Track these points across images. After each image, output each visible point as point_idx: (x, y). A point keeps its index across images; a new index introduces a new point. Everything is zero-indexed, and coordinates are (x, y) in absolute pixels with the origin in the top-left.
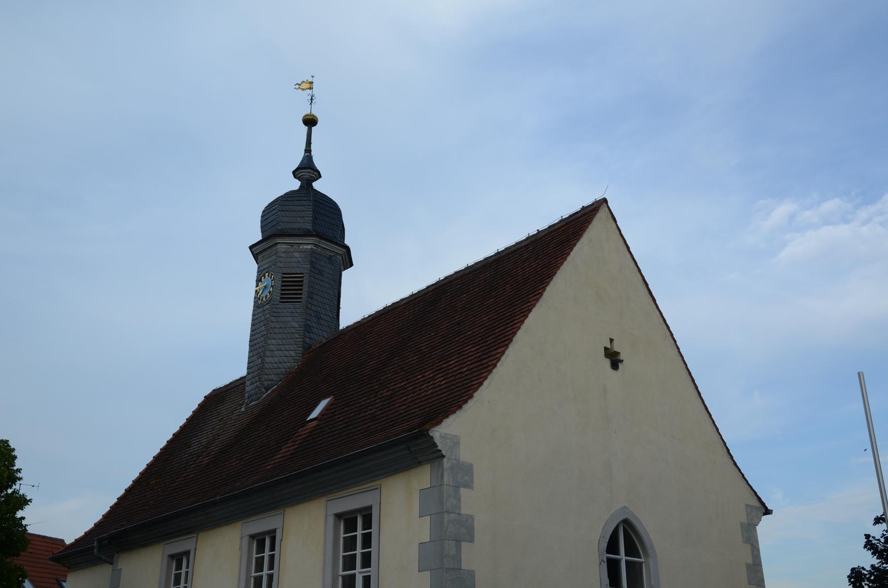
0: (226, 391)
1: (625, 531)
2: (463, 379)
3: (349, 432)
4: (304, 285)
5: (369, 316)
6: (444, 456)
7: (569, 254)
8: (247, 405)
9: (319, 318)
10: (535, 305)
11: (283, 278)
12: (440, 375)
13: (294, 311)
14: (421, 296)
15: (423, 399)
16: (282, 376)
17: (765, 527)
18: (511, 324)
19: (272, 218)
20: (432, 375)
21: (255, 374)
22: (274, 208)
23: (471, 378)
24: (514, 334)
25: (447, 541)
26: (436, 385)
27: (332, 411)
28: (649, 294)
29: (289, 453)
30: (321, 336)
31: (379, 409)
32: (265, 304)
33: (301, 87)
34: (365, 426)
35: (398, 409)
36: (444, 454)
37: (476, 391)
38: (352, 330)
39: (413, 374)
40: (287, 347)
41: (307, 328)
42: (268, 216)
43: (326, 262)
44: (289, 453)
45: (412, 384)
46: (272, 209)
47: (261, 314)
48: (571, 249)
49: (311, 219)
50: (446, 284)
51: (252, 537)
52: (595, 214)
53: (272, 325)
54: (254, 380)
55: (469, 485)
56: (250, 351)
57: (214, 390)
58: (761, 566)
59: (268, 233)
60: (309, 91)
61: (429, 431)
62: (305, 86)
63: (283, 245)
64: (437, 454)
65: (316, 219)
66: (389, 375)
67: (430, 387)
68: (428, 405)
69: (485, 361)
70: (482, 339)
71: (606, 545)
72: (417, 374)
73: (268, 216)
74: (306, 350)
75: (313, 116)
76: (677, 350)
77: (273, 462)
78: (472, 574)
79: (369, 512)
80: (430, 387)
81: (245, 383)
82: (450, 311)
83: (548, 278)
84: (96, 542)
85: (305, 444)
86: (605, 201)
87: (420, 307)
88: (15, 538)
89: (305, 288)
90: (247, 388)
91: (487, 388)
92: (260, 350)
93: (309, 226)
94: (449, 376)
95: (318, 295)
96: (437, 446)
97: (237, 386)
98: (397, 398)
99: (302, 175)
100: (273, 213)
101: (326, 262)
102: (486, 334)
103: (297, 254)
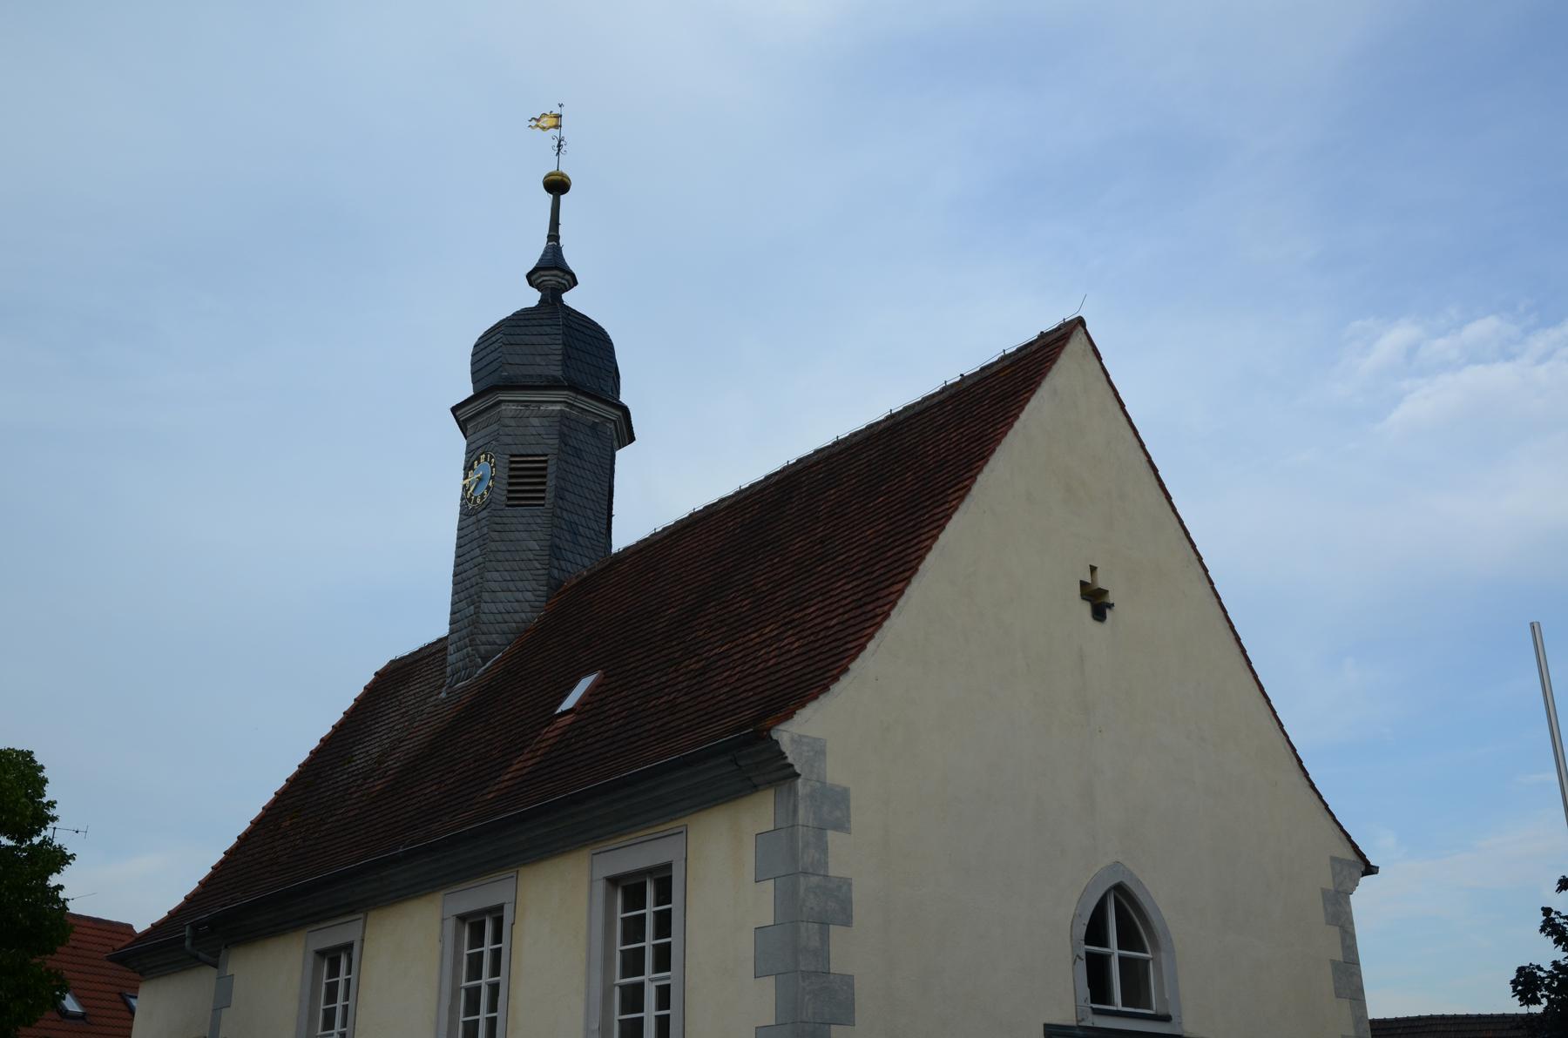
0: (412, 663)
3: (630, 733)
4: (549, 476)
5: (664, 529)
6: (798, 775)
7: (1016, 417)
8: (450, 687)
9: (575, 533)
13: (531, 521)
14: (756, 494)
15: (760, 675)
17: (1365, 897)
19: (491, 357)
20: (775, 633)
22: (494, 339)
25: (805, 924)
30: (579, 564)
31: (683, 692)
32: (480, 509)
33: (540, 124)
36: (798, 771)
40: (520, 584)
41: (555, 551)
42: (484, 352)
44: (525, 771)
45: (740, 648)
48: (1022, 408)
50: (799, 471)
51: (462, 918)
52: (1064, 345)
53: (493, 546)
55: (842, 826)
56: (455, 593)
58: (1359, 964)
59: (483, 385)
60: (556, 132)
62: (547, 122)
66: (701, 633)
67: (773, 654)
69: (870, 607)
72: (749, 631)
73: (484, 352)
74: (551, 588)
75: (562, 175)
76: (1209, 586)
78: (848, 980)
79: (668, 874)
80: (773, 654)
84: (188, 928)
86: (1080, 322)
87: (754, 512)
89: (551, 482)
90: (449, 658)
92: (472, 591)
94: (805, 634)
96: (786, 757)
97: (430, 657)
99: (544, 281)
100: (492, 348)
103: (535, 422)
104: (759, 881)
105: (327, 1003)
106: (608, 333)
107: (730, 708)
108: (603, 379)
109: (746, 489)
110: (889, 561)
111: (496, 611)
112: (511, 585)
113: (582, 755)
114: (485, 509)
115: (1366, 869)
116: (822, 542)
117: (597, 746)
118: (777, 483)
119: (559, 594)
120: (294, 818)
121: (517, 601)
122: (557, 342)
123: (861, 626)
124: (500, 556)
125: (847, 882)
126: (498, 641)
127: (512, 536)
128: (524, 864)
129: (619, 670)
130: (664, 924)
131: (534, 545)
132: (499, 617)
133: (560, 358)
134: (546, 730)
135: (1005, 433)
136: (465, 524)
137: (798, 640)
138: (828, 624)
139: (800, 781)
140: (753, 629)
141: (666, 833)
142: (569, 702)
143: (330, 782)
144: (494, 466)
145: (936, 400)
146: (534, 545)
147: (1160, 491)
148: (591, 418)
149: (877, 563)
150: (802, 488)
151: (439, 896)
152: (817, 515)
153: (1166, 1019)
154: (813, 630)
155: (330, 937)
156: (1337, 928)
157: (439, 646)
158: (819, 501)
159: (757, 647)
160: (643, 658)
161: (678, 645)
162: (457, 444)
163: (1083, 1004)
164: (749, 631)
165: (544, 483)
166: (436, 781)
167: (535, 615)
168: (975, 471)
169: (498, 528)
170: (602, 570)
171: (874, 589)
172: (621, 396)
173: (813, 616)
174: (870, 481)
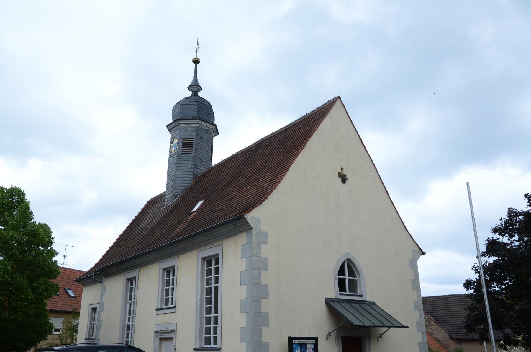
0: (157, 198)
1: (348, 264)
2: (264, 189)
3: (210, 217)
4: (194, 143)
5: (225, 159)
6: (252, 228)
7: (319, 125)
8: (166, 205)
9: (201, 161)
10: (301, 151)
11: (183, 141)
12: (254, 188)
13: (188, 157)
14: (250, 149)
15: (245, 200)
16: (183, 190)
17: (422, 261)
18: (289, 161)
20: (250, 188)
21: (170, 190)
22: (178, 106)
23: (268, 189)
24: (290, 166)
25: (254, 270)
26: (252, 193)
27: (204, 207)
28: (362, 145)
29: (182, 228)
30: (202, 170)
31: (225, 205)
34: (217, 214)
35: (233, 205)
36: (252, 227)
37: (269, 195)
38: (216, 167)
39: (242, 188)
40: (185, 176)
41: (195, 166)
42: (175, 110)
43: (205, 133)
44: (182, 228)
45: (241, 192)
46: (177, 106)
47: (173, 160)
48: (321, 122)
49: (197, 111)
50: (262, 142)
51: (164, 269)
52: (334, 104)
54: (170, 192)
55: (265, 242)
56: (168, 178)
57: (152, 198)
58: (419, 280)
59: (174, 120)
61: (244, 216)
63: (183, 124)
64: (249, 227)
65: (199, 111)
66: (231, 189)
67: (249, 194)
68: (247, 203)
69: (275, 180)
70: (275, 169)
71: (338, 271)
72: (244, 188)
73: (175, 110)
74: (194, 177)
75: (198, 58)
76: (377, 173)
77: (175, 233)
78: (267, 286)
79: (218, 257)
80: (249, 194)
81: (165, 195)
82: (262, 156)
83: (308, 138)
84: (93, 273)
85: (190, 224)
86: (339, 97)
87: (249, 154)
88: (53, 270)
89: (194, 146)
90: (166, 197)
91: (275, 194)
92: (172, 178)
93: (196, 115)
94: (258, 188)
95: (201, 149)
96: (249, 223)
97: (162, 197)
98: (233, 200)
99: (192, 89)
101: (205, 133)
102: (277, 166)
103: (190, 129)
104: (242, 258)
105: (130, 293)
106: (211, 103)
107: (236, 209)
108: (209, 117)
109: (247, 148)
110: (282, 167)
111: (179, 183)
112: (183, 176)
113: (197, 223)
114: (176, 154)
115: (422, 253)
116: (265, 162)
117: (201, 221)
118: (256, 145)
119: (196, 178)
120: (124, 242)
121: (185, 180)
122: (196, 106)
123: (272, 186)
124: (180, 168)
125: (267, 259)
126: (179, 192)
127: (183, 162)
128: (181, 254)
129: (209, 199)
130: (217, 270)
131: (189, 164)
132: (180, 185)
134: (189, 217)
135: (316, 130)
136: (170, 159)
137: (256, 190)
138: (264, 185)
139: (253, 230)
140: (245, 187)
141: (218, 245)
142: (195, 209)
143: (134, 232)
144: (178, 142)
145: (299, 121)
146: (189, 164)
147: (363, 146)
148: (206, 128)
149: (279, 167)
150: (262, 147)
151: (158, 264)
152: (265, 154)
153: (362, 296)
154: (260, 187)
155: (130, 275)
156: (413, 270)
157: (164, 194)
158: (266, 150)
159: (245, 192)
160: (216, 196)
161: (225, 192)
162: (168, 135)
163: (337, 292)
164: (244, 188)
165: (192, 147)
166: (160, 231)
167: (190, 184)
168: (307, 141)
169: (179, 160)
170: (208, 171)
171: (277, 175)
172: (215, 121)
173: (260, 183)
174: (279, 144)
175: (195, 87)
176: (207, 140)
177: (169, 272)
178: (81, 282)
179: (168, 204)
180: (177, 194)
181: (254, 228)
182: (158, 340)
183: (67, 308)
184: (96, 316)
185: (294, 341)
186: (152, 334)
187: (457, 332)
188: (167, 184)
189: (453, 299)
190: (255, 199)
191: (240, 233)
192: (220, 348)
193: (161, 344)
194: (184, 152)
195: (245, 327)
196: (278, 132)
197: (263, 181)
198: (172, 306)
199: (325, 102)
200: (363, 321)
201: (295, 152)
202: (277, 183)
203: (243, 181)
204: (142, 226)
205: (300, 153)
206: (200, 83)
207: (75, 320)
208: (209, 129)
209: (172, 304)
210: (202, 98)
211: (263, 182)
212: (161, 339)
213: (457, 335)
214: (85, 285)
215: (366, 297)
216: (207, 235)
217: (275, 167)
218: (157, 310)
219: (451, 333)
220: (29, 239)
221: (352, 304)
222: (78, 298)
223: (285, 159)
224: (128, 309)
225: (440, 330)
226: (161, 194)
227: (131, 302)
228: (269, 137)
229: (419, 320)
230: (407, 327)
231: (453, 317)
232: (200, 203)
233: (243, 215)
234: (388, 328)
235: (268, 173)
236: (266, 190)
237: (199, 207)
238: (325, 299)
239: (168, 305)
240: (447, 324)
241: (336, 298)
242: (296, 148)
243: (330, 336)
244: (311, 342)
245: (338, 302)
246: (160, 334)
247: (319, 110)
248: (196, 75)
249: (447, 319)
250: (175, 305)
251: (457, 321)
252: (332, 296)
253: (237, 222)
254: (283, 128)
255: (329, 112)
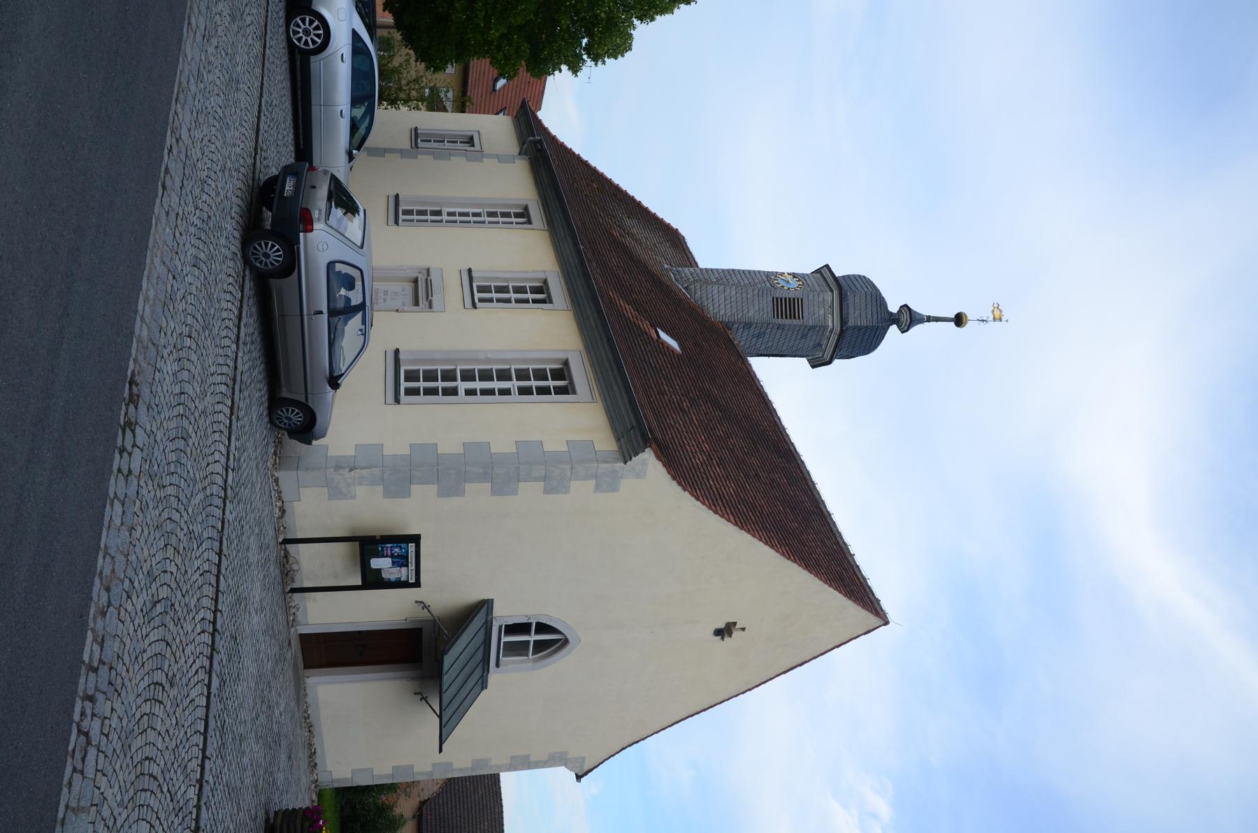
0: (683, 248)
1: (556, 641)
5: (762, 386)
6: (625, 463)
11: (798, 299)
12: (705, 458)
13: (765, 311)
14: (783, 437)
15: (681, 441)
17: (564, 775)
21: (701, 276)
24: (748, 532)
26: (695, 454)
29: (625, 312)
30: (741, 339)
33: (996, 310)
36: (628, 463)
39: (705, 431)
41: (748, 325)
42: (860, 281)
44: (625, 312)
46: (867, 285)
47: (760, 279)
48: (836, 589)
50: (797, 463)
53: (750, 291)
55: (598, 488)
56: (723, 271)
57: (684, 238)
59: (842, 282)
62: (997, 313)
64: (628, 458)
65: (859, 330)
69: (720, 503)
73: (860, 281)
75: (966, 323)
76: (734, 694)
78: (515, 492)
80: (693, 449)
84: (539, 138)
85: (634, 328)
86: (887, 623)
89: (787, 322)
90: (687, 269)
96: (635, 456)
97: (687, 258)
98: (681, 415)
102: (747, 503)
103: (822, 312)
109: (786, 432)
110: (747, 514)
112: (728, 301)
118: (790, 450)
124: (744, 295)
126: (697, 295)
133: (859, 324)
136: (762, 274)
139: (622, 464)
142: (663, 336)
144: (796, 290)
145: (840, 540)
149: (745, 507)
153: (498, 665)
154: (707, 471)
162: (807, 267)
165: (786, 318)
167: (712, 315)
169: (761, 292)
175: (908, 319)
176: (801, 345)
177: (541, 292)
178: (521, 113)
179: (673, 274)
180: (693, 290)
181: (625, 466)
182: (415, 275)
183: (474, 77)
184: (459, 146)
185: (414, 544)
186: (426, 264)
187: (433, 814)
188: (712, 270)
189: (495, 808)
190: (682, 463)
191: (615, 438)
192: (399, 403)
193: (410, 282)
194: (775, 302)
195: (439, 453)
196: (817, 495)
197: (719, 476)
198: (476, 301)
199: (878, 594)
200: (450, 671)
201: (776, 541)
202: (715, 507)
203: (719, 430)
204: (629, 222)
205: (775, 550)
206: (916, 329)
207: (451, 103)
208: (822, 349)
209: (481, 300)
210: (885, 334)
211: (717, 476)
212: (416, 281)
213: (429, 813)
214: (517, 120)
215: (495, 672)
216: (612, 370)
217: (746, 497)
218: (470, 271)
219: (433, 803)
220: (602, 19)
221: (482, 647)
222: (493, 95)
223: (762, 518)
224: (471, 210)
225: (438, 783)
226: (693, 257)
227: (484, 216)
228: (808, 477)
229: (454, 767)
230: (441, 751)
231: (462, 809)
232: (674, 344)
233: (650, 447)
234: (438, 714)
235: (734, 484)
236: (700, 486)
237: (666, 342)
238: (491, 598)
239: (478, 292)
240: (449, 795)
241: (494, 619)
242: (784, 540)
243: (423, 609)
244: (412, 576)
245: (486, 622)
246: (424, 278)
247: (862, 580)
248: (933, 321)
249: (457, 796)
250: (477, 306)
251: (454, 815)
252: (498, 611)
253: (638, 434)
254: (825, 507)
255: (858, 604)
